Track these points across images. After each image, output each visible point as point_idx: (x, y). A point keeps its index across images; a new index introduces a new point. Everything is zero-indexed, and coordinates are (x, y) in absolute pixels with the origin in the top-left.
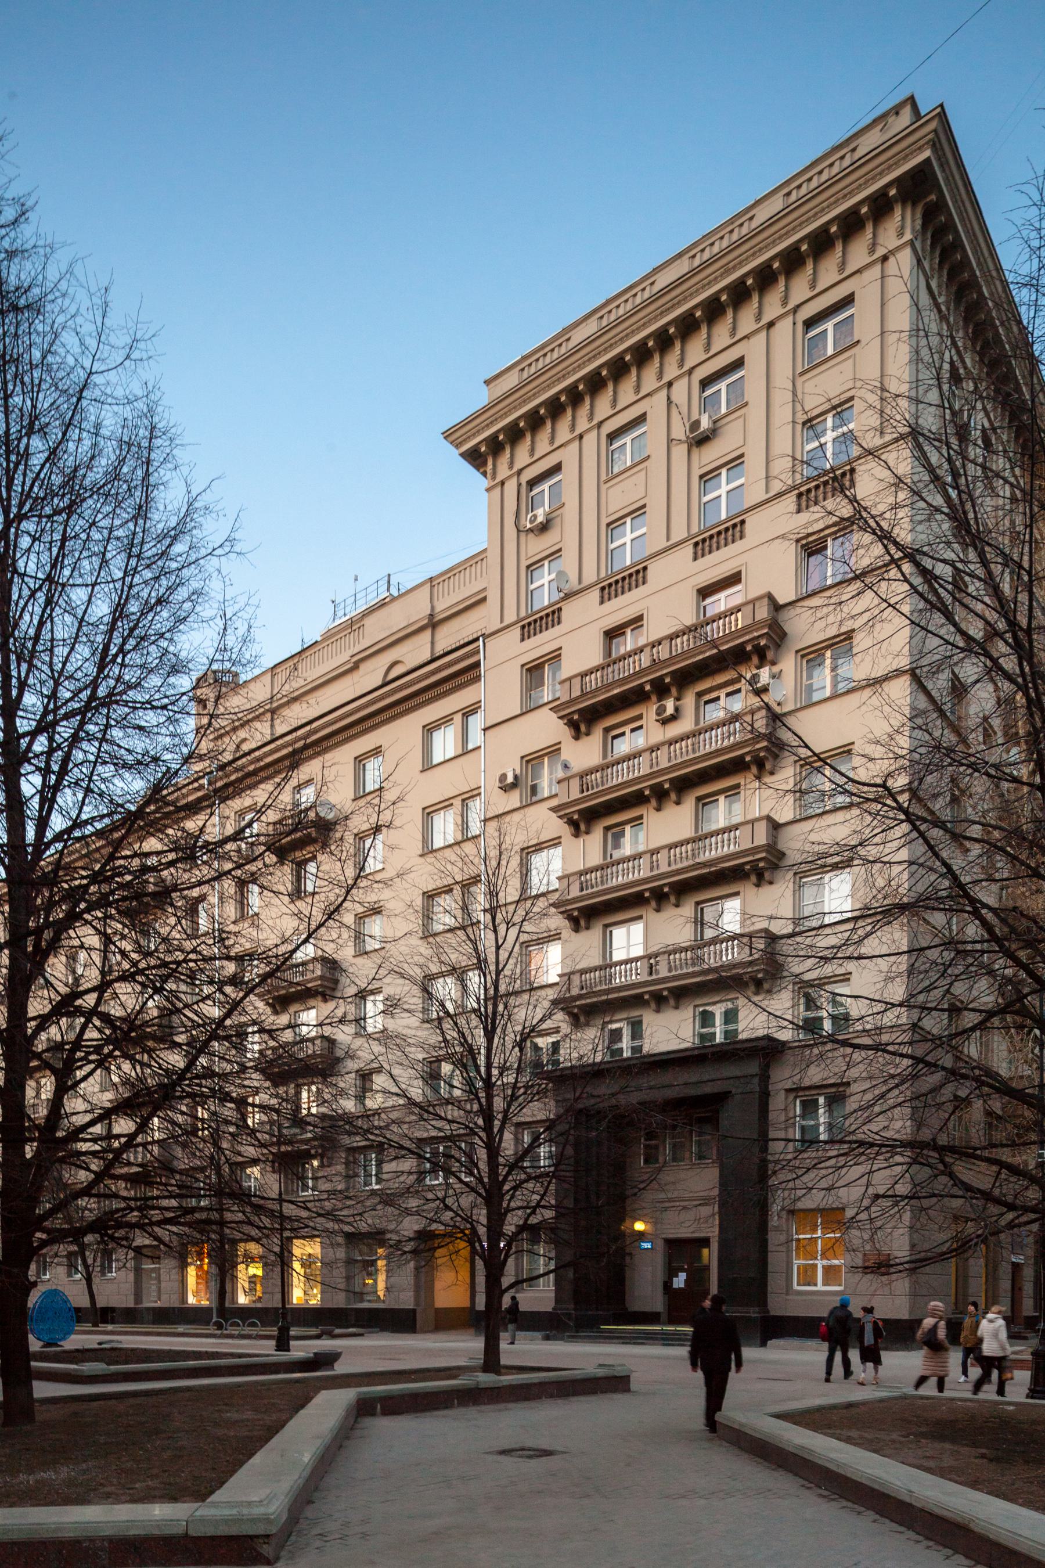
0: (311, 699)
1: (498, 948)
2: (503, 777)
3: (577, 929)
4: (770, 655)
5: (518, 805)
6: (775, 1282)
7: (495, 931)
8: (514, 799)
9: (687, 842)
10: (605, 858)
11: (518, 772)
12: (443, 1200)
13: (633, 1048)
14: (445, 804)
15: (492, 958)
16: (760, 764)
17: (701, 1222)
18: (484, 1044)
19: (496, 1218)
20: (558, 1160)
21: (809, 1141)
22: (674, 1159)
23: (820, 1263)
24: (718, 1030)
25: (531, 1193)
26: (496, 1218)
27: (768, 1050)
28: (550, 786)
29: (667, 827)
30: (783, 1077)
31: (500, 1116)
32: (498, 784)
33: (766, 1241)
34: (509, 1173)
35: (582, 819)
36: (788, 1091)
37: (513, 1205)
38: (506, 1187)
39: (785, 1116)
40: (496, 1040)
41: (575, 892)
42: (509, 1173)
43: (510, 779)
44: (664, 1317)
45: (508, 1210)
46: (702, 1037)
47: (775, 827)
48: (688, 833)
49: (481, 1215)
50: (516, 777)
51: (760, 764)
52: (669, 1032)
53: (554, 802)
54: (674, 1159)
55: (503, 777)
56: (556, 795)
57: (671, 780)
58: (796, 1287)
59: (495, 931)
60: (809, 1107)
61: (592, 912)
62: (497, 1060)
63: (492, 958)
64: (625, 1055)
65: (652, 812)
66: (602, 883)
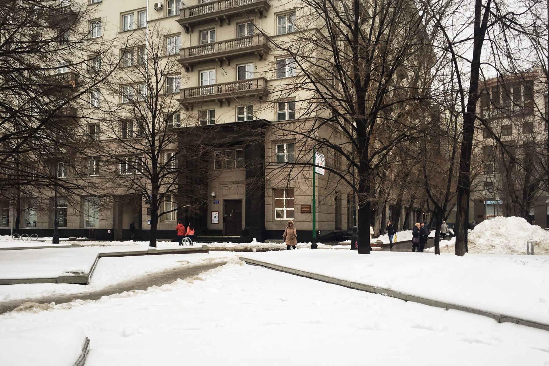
0: (243, 248)
1: (157, 83)
2: (156, 5)
3: (187, 70)
4: (265, 13)
5: (163, 17)
6: (268, 217)
7: (157, 77)
8: (161, 15)
9: (233, 40)
10: (199, 44)
11: (163, 3)
12: (133, 180)
13: (211, 121)
14: (131, 12)
15: (155, 87)
16: (261, 98)
17: (238, 192)
18: (151, 120)
19: (156, 187)
20: (179, 166)
21: (280, 160)
22: (228, 168)
23: (285, 209)
24: (245, 116)
25: (169, 179)
26: (156, 187)
27: (264, 124)
28: (176, 11)
29: (226, 34)
30: (271, 137)
31: (158, 148)
32: (154, 7)
33: (264, 202)
34: (160, 171)
35: (189, 26)
36: (273, 141)
37: (162, 183)
38: (160, 176)
39: (272, 153)
40: (156, 119)
41: (187, 56)
42: (160, 171)
43: (159, 6)
44: (224, 232)
45: (160, 185)
46: (239, 119)
47: (266, 81)
48: (233, 37)
49: (149, 187)
50: (162, 5)
51: (261, 98)
52: (226, 116)
53: (178, 18)
54: (228, 168)
55: (156, 5)
56: (179, 15)
57: (226, 15)
58: (276, 219)
59: (157, 77)
60: (280, 148)
61: (193, 64)
62: (157, 126)
63: (155, 87)
64: (208, 124)
65: (218, 26)
66: (198, 53)
